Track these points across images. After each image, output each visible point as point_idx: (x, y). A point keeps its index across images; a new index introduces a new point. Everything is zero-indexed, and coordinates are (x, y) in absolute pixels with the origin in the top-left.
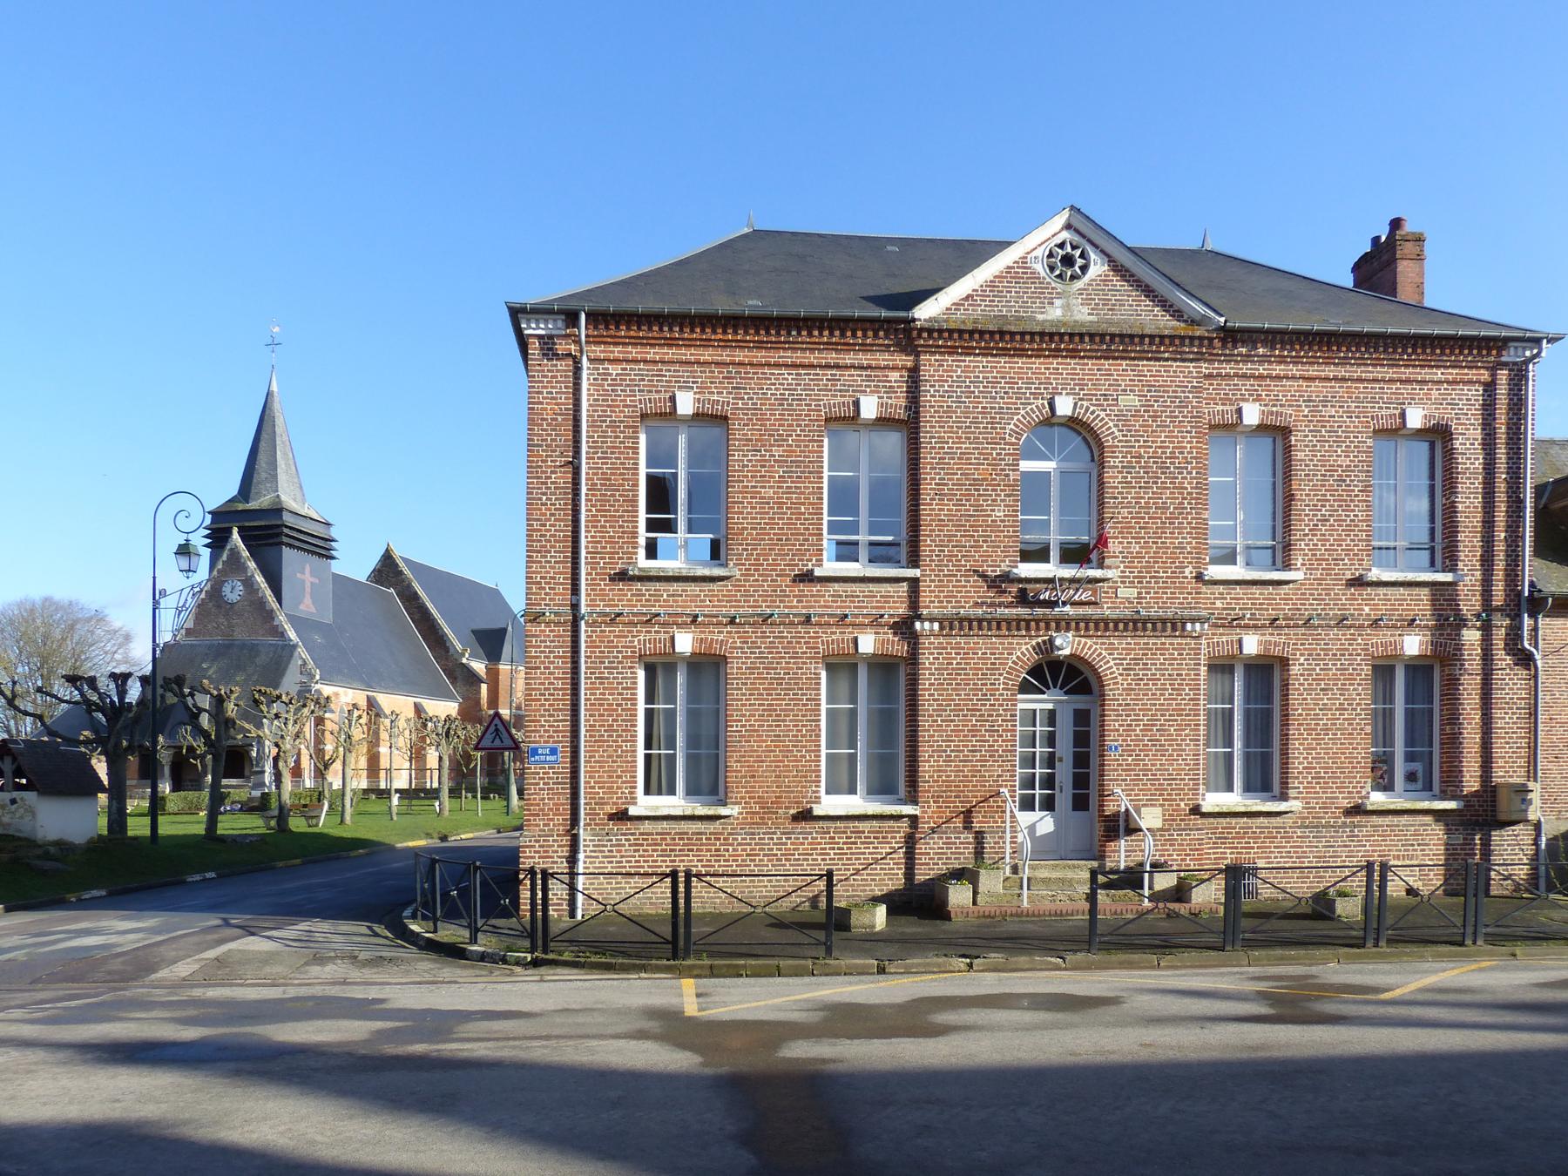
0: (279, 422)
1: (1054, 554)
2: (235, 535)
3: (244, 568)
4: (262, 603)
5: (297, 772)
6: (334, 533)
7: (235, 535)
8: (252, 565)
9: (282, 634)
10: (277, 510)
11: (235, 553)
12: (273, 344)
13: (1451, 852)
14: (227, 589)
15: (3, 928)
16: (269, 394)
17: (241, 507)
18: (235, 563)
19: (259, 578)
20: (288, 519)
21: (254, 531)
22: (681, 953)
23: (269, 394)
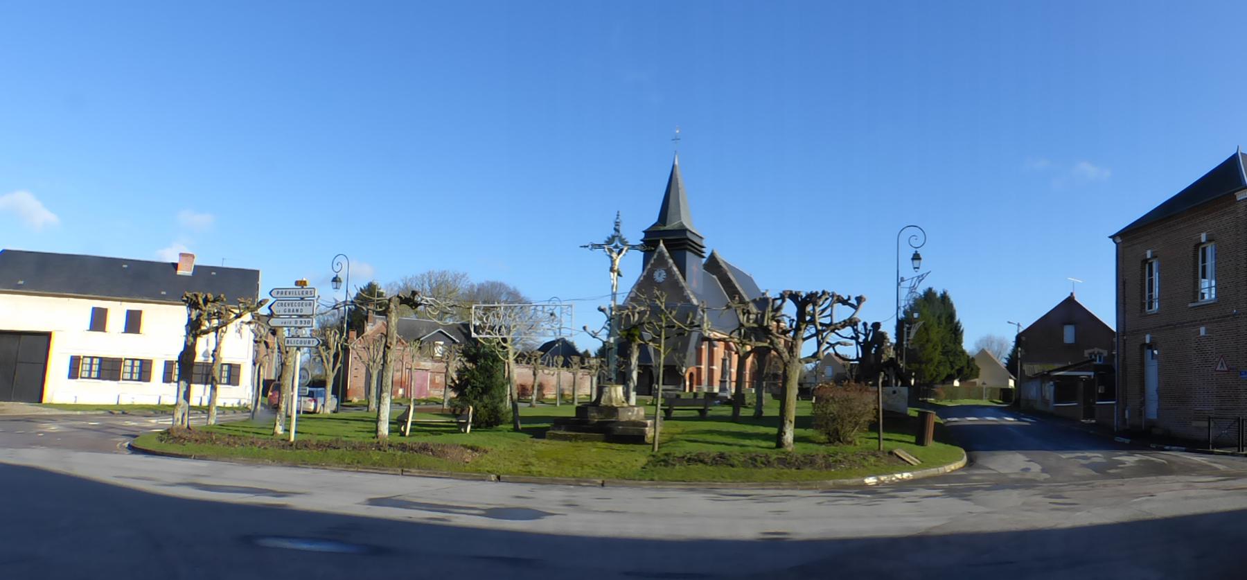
0: (680, 181)
1: (158, 371)
2: (662, 244)
3: (667, 262)
4: (677, 282)
5: (699, 382)
6: (704, 243)
7: (662, 244)
8: (671, 261)
9: (689, 301)
10: (684, 230)
11: (661, 254)
12: (676, 139)
13: (960, 342)
14: (656, 274)
15: (40, 228)
16: (674, 166)
17: (662, 228)
18: (661, 261)
19: (675, 269)
20: (689, 235)
21: (668, 241)
22: (802, 432)
23: (674, 166)
